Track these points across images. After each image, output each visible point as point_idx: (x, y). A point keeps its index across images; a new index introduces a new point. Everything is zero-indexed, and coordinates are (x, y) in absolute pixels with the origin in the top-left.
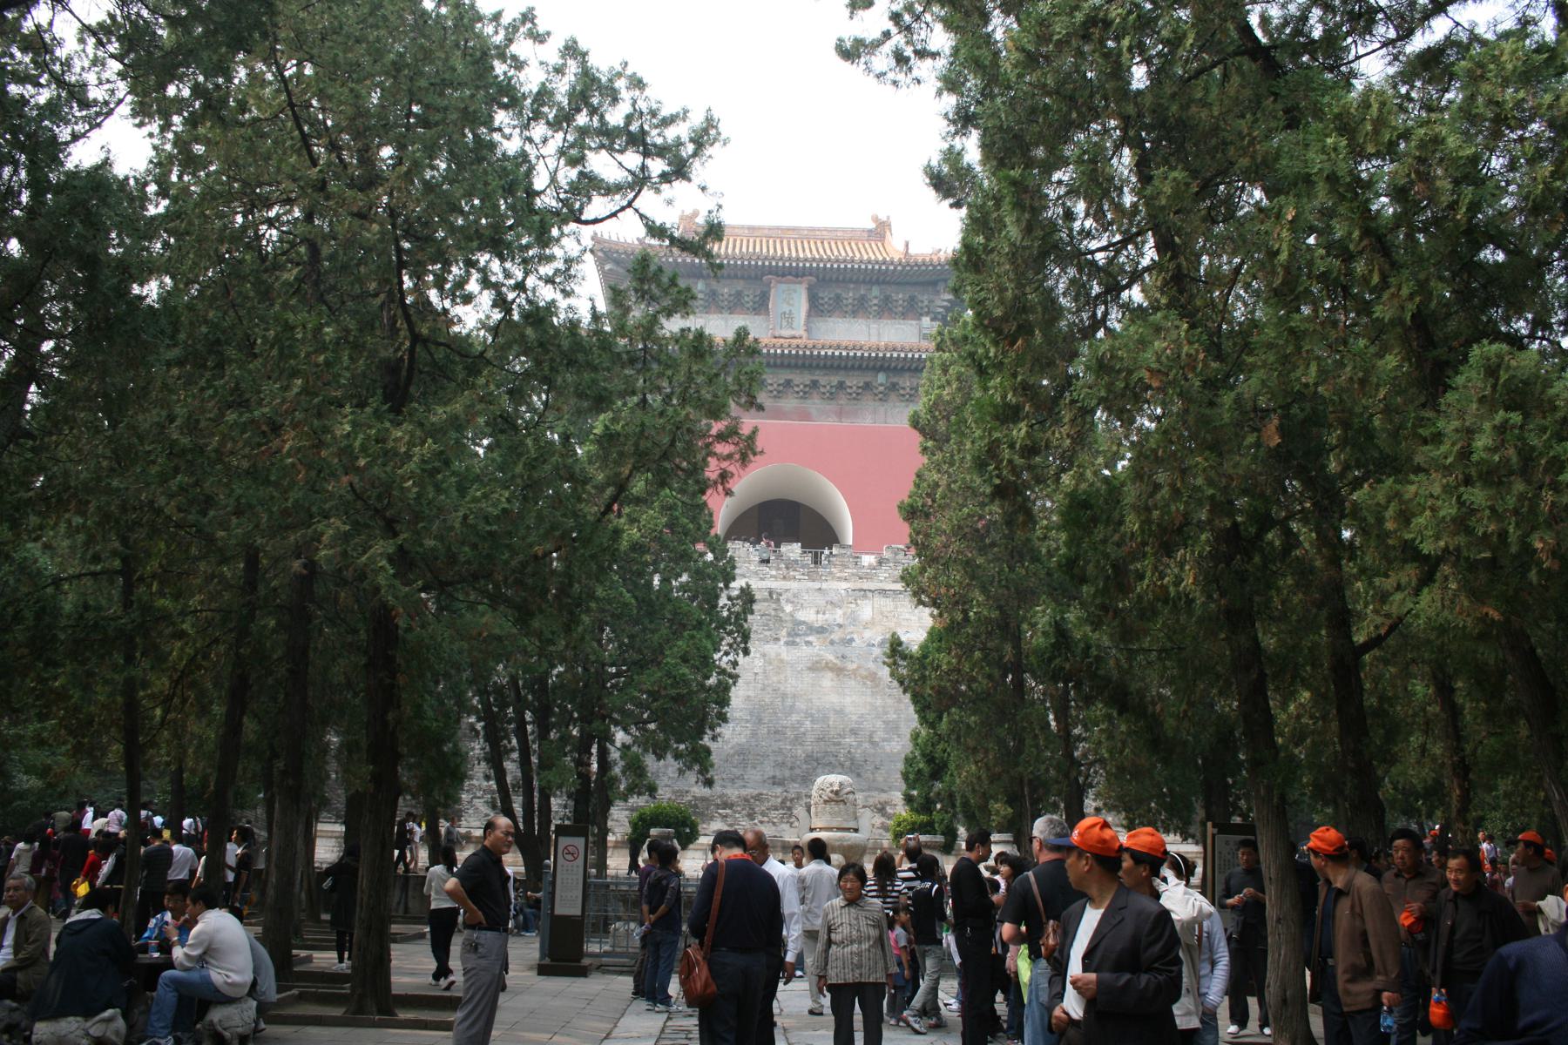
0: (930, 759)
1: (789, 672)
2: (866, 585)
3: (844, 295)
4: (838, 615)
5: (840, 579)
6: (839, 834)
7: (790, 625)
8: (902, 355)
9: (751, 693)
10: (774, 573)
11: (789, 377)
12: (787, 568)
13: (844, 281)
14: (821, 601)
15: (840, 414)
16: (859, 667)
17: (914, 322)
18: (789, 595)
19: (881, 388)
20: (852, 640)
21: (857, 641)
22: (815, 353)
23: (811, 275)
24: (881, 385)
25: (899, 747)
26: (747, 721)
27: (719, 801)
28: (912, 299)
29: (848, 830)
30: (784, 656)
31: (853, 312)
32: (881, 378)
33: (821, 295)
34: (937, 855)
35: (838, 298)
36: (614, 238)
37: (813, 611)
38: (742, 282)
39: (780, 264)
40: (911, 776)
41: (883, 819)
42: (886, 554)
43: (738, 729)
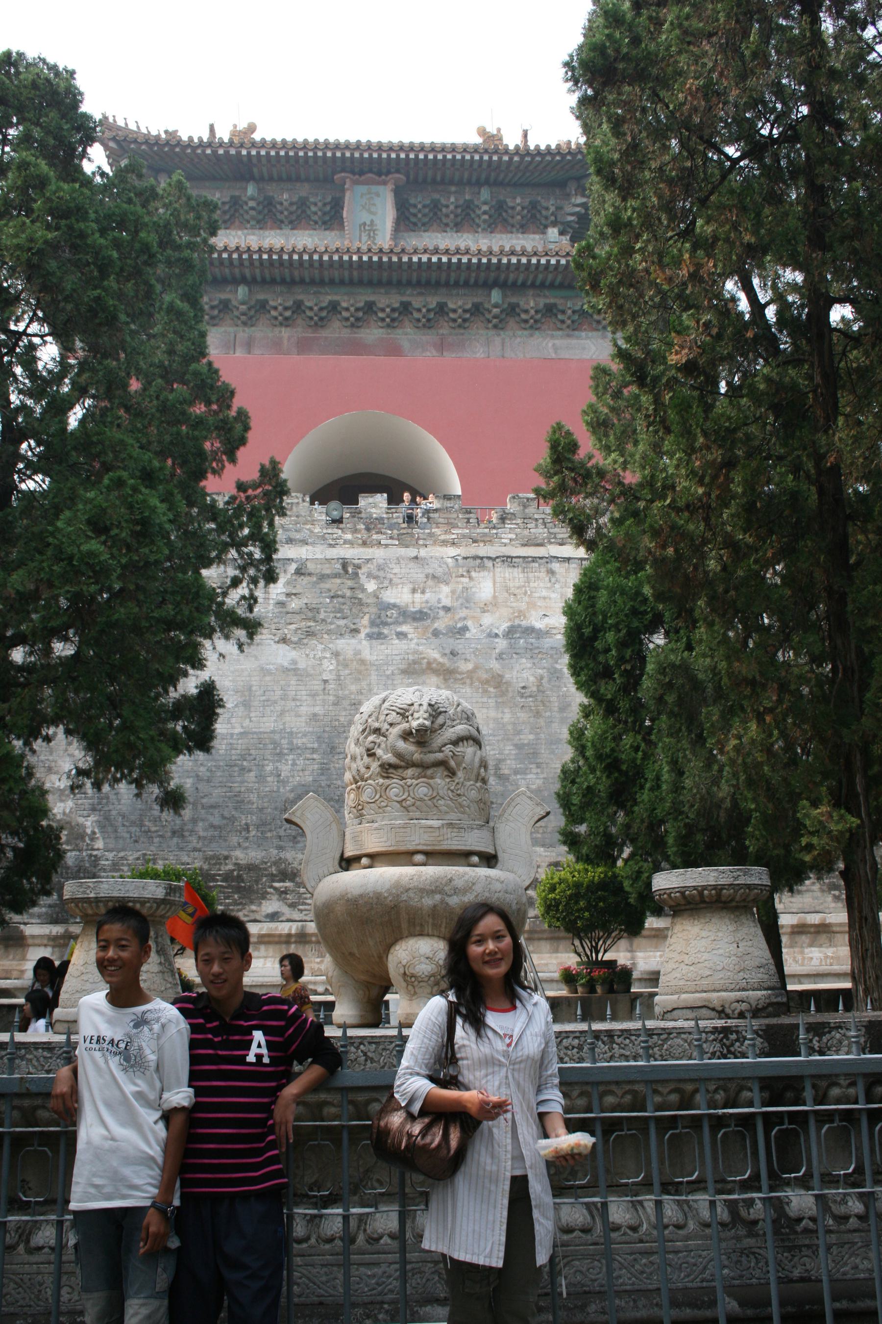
0: (612, 764)
1: (374, 677)
2: (483, 550)
3: (443, 201)
4: (444, 594)
5: (445, 543)
6: (432, 872)
7: (373, 610)
8: (524, 260)
9: (318, 710)
10: (349, 536)
11: (372, 298)
12: (368, 529)
13: (442, 182)
14: (417, 574)
15: (441, 347)
16: (476, 668)
17: (537, 237)
18: (371, 567)
19: (496, 311)
20: (465, 629)
21: (474, 631)
22: (405, 259)
23: (398, 171)
24: (496, 306)
25: (539, 782)
26: (314, 751)
27: (274, 870)
28: (534, 205)
29: (462, 856)
30: (367, 655)
31: (456, 225)
32: (496, 296)
33: (412, 201)
34: (153, 949)
35: (435, 206)
36: (132, 127)
37: (407, 589)
38: (306, 185)
40: (576, 800)
43: (300, 762)
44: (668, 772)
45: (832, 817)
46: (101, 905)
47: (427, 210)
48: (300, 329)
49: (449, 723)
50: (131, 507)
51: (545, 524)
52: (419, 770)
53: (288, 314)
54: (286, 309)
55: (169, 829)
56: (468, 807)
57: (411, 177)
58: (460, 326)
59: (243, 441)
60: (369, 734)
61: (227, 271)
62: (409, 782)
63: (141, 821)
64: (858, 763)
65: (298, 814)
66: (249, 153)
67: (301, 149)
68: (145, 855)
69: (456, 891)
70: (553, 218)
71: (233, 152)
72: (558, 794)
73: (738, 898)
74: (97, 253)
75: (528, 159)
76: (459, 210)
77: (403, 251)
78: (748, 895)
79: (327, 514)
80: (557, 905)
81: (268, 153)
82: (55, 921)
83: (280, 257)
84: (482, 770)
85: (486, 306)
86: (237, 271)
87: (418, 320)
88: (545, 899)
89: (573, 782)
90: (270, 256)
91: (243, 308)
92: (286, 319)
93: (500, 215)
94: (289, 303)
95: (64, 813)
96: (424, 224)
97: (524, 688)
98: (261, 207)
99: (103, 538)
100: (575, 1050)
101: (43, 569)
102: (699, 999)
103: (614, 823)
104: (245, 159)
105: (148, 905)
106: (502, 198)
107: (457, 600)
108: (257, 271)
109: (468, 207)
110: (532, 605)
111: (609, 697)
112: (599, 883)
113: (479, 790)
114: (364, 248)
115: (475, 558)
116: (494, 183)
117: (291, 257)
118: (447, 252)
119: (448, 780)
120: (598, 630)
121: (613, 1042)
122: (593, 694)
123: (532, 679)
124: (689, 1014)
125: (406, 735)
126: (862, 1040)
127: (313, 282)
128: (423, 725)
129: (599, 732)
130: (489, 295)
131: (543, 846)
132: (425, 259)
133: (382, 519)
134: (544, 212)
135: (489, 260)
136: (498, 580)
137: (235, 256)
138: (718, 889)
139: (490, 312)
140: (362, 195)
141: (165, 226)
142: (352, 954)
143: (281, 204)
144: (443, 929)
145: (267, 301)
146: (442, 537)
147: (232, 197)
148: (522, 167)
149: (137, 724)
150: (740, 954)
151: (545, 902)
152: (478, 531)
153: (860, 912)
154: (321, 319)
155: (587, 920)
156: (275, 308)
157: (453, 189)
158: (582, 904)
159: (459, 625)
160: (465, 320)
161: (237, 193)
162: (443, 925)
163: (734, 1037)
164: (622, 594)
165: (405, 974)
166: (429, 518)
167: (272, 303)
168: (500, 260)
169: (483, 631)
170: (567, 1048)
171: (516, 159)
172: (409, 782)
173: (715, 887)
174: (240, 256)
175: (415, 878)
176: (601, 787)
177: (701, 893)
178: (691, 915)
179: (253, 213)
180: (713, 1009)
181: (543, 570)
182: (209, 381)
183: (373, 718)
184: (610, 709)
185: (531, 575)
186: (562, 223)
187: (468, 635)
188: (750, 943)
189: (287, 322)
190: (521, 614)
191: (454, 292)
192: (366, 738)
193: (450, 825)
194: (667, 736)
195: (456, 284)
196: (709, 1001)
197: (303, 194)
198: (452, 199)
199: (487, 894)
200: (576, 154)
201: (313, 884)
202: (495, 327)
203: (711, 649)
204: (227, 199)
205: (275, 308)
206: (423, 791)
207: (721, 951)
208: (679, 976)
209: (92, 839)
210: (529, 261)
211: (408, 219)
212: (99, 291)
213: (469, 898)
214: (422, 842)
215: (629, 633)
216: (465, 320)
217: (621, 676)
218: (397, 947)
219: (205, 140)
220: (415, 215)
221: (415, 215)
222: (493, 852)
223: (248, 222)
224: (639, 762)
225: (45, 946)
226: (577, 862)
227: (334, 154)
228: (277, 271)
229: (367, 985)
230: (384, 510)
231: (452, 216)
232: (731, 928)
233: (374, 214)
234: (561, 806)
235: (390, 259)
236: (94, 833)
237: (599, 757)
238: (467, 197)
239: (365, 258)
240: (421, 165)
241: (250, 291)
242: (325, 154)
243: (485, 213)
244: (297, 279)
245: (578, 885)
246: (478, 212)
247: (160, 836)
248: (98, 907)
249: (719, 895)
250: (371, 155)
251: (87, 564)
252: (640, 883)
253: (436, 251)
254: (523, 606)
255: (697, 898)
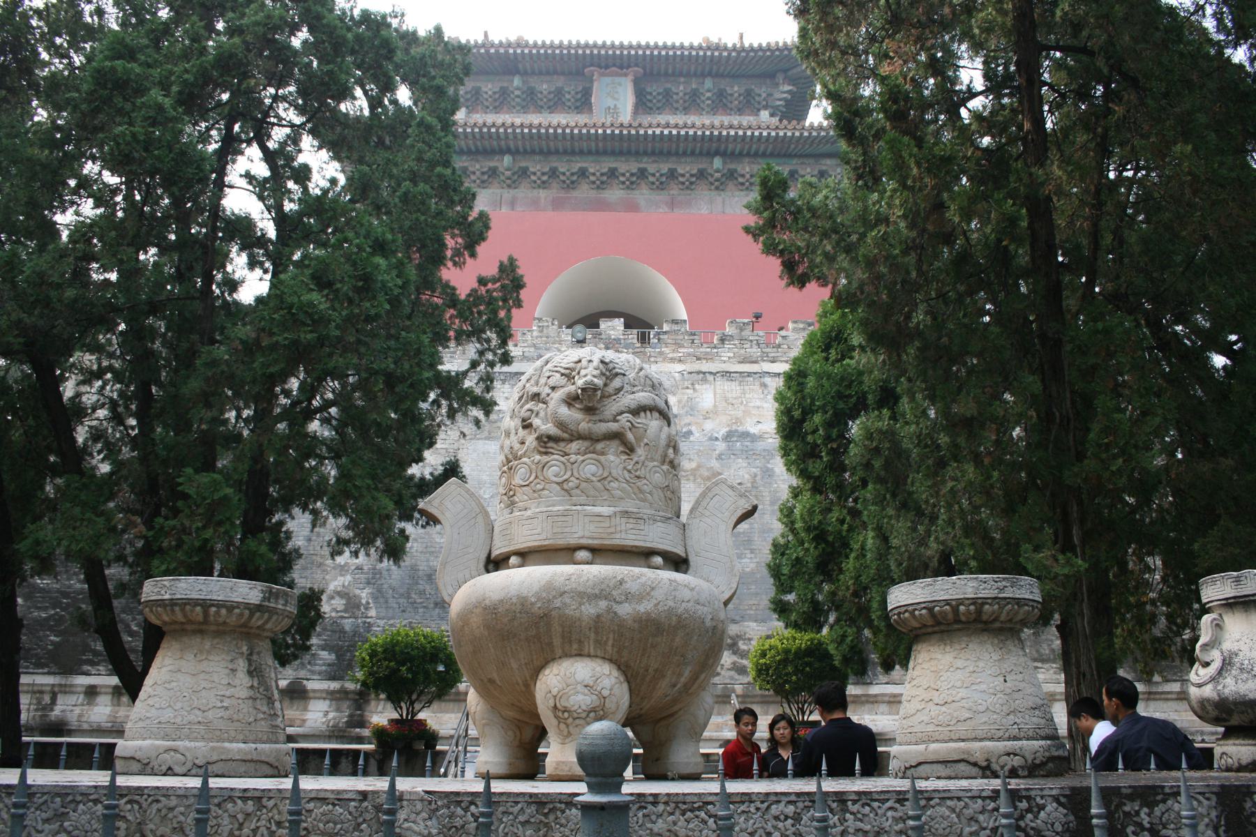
0: (820, 535)
2: (705, 366)
3: (674, 90)
5: (672, 360)
11: (614, 165)
13: (673, 74)
15: (672, 204)
16: (699, 467)
20: (690, 433)
22: (642, 132)
23: (637, 65)
25: (753, 566)
29: (643, 555)
31: (685, 109)
32: (717, 162)
33: (649, 90)
35: (667, 94)
38: (562, 78)
39: (603, 52)
40: (785, 570)
41: (735, 658)
42: (729, 330)
44: (873, 538)
45: (1057, 560)
46: (177, 609)
47: (660, 97)
48: (555, 191)
49: (627, 388)
50: (354, 264)
51: (758, 344)
52: (587, 444)
53: (545, 178)
54: (543, 174)
55: (432, 600)
56: (650, 493)
57: (648, 71)
58: (687, 188)
59: (481, 237)
60: (527, 402)
61: (495, 143)
62: (573, 458)
63: (409, 593)
64: (1075, 515)
65: (436, 503)
66: (515, 52)
67: (558, 48)
68: (411, 623)
69: (628, 597)
70: (764, 103)
71: (502, 51)
72: (769, 566)
73: (1003, 618)
74: (332, 33)
75: (743, 54)
76: (687, 97)
77: (640, 125)
78: (1017, 613)
79: (573, 336)
80: (767, 670)
81: (530, 52)
82: (333, 678)
83: (539, 131)
84: (671, 451)
85: (709, 171)
86: (503, 143)
87: (653, 183)
88: (757, 664)
89: (783, 554)
90: (530, 130)
91: (508, 173)
92: (544, 182)
93: (721, 101)
94: (546, 169)
95: (344, 586)
96: (658, 108)
97: (740, 484)
98: (524, 96)
99: (326, 292)
100: (790, 821)
101: (263, 318)
102: (955, 749)
103: (820, 590)
104: (512, 57)
105: (237, 611)
106: (722, 87)
107: (683, 408)
108: (520, 143)
109: (695, 94)
110: (747, 413)
111: (817, 474)
112: (806, 650)
113: (665, 474)
114: (608, 124)
115: (699, 372)
116: (718, 75)
117: (547, 131)
118: (676, 126)
119: (624, 457)
120: (807, 412)
121: (845, 810)
122: (803, 474)
123: (747, 476)
124: (941, 770)
125: (571, 400)
126: (1214, 814)
127: (565, 152)
128: (591, 383)
129: (808, 506)
130: (712, 163)
131: (756, 621)
132: (658, 132)
133: (619, 339)
134: (757, 98)
135: (712, 133)
136: (718, 391)
137: (501, 130)
138: (978, 603)
139: (712, 176)
140: (607, 85)
141: (421, 59)
142: (491, 681)
143: (541, 93)
144: (609, 648)
145: (527, 168)
146: (671, 355)
147: (501, 88)
148: (738, 61)
149: (354, 472)
150: (1008, 691)
151: (757, 666)
152: (701, 350)
153: (1078, 667)
154: (573, 182)
155: (795, 683)
156: (535, 174)
157: (682, 79)
158: (790, 669)
159: (684, 430)
160: (691, 183)
161: (505, 85)
162: (610, 643)
163: (1024, 805)
164: (828, 379)
165: (555, 707)
166: (659, 339)
167: (532, 170)
168: (720, 133)
169: (705, 435)
170: (777, 818)
171: (734, 54)
172: (573, 458)
173: (974, 601)
174: (506, 130)
175: (573, 577)
176: (809, 559)
177: (955, 610)
178: (941, 640)
179: (518, 100)
180: (975, 764)
181: (757, 383)
182: (452, 183)
183: (532, 382)
184: (818, 487)
185: (747, 388)
186: (772, 107)
187: (692, 438)
188: (1020, 677)
189: (544, 185)
190: (738, 421)
191: (683, 160)
192: (522, 407)
193: (626, 514)
194: (872, 504)
195: (684, 154)
196: (968, 752)
197: (560, 84)
198: (681, 88)
199: (671, 603)
200: (783, 50)
201: (450, 591)
202: (717, 188)
203: (916, 416)
204: (497, 90)
205: (535, 174)
206: (590, 469)
207: (983, 687)
208: (926, 719)
209: (366, 609)
210: (745, 133)
211: (645, 104)
212: (332, 66)
213: (644, 607)
214: (587, 534)
215: (835, 414)
216: (691, 183)
217: (828, 454)
218: (547, 671)
219: (480, 42)
220: (650, 101)
221: (650, 101)
222: (683, 555)
223: (514, 107)
224: (844, 534)
225: (324, 699)
226: (786, 627)
227: (584, 52)
228: (536, 142)
229: (518, 725)
230: (621, 332)
231: (681, 101)
232: (995, 657)
233: (617, 99)
234: (772, 576)
235: (629, 132)
236: (368, 603)
237: (808, 529)
238: (694, 86)
239: (609, 131)
240: (655, 60)
241: (514, 159)
242: (577, 52)
243: (708, 99)
244: (553, 149)
245: (787, 651)
246: (703, 98)
247: (425, 607)
248: (173, 611)
249: (979, 612)
250: (614, 52)
251: (306, 312)
252: (845, 646)
253: (667, 126)
254: (740, 414)
255: (950, 616)
